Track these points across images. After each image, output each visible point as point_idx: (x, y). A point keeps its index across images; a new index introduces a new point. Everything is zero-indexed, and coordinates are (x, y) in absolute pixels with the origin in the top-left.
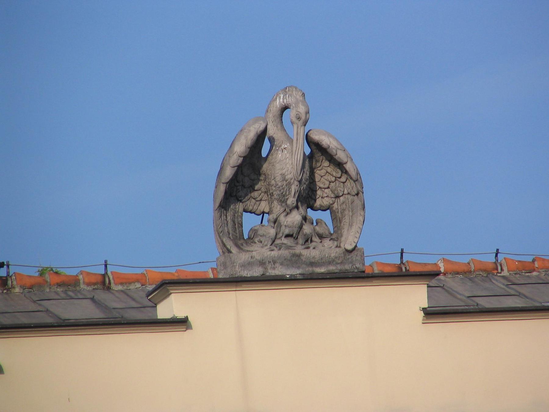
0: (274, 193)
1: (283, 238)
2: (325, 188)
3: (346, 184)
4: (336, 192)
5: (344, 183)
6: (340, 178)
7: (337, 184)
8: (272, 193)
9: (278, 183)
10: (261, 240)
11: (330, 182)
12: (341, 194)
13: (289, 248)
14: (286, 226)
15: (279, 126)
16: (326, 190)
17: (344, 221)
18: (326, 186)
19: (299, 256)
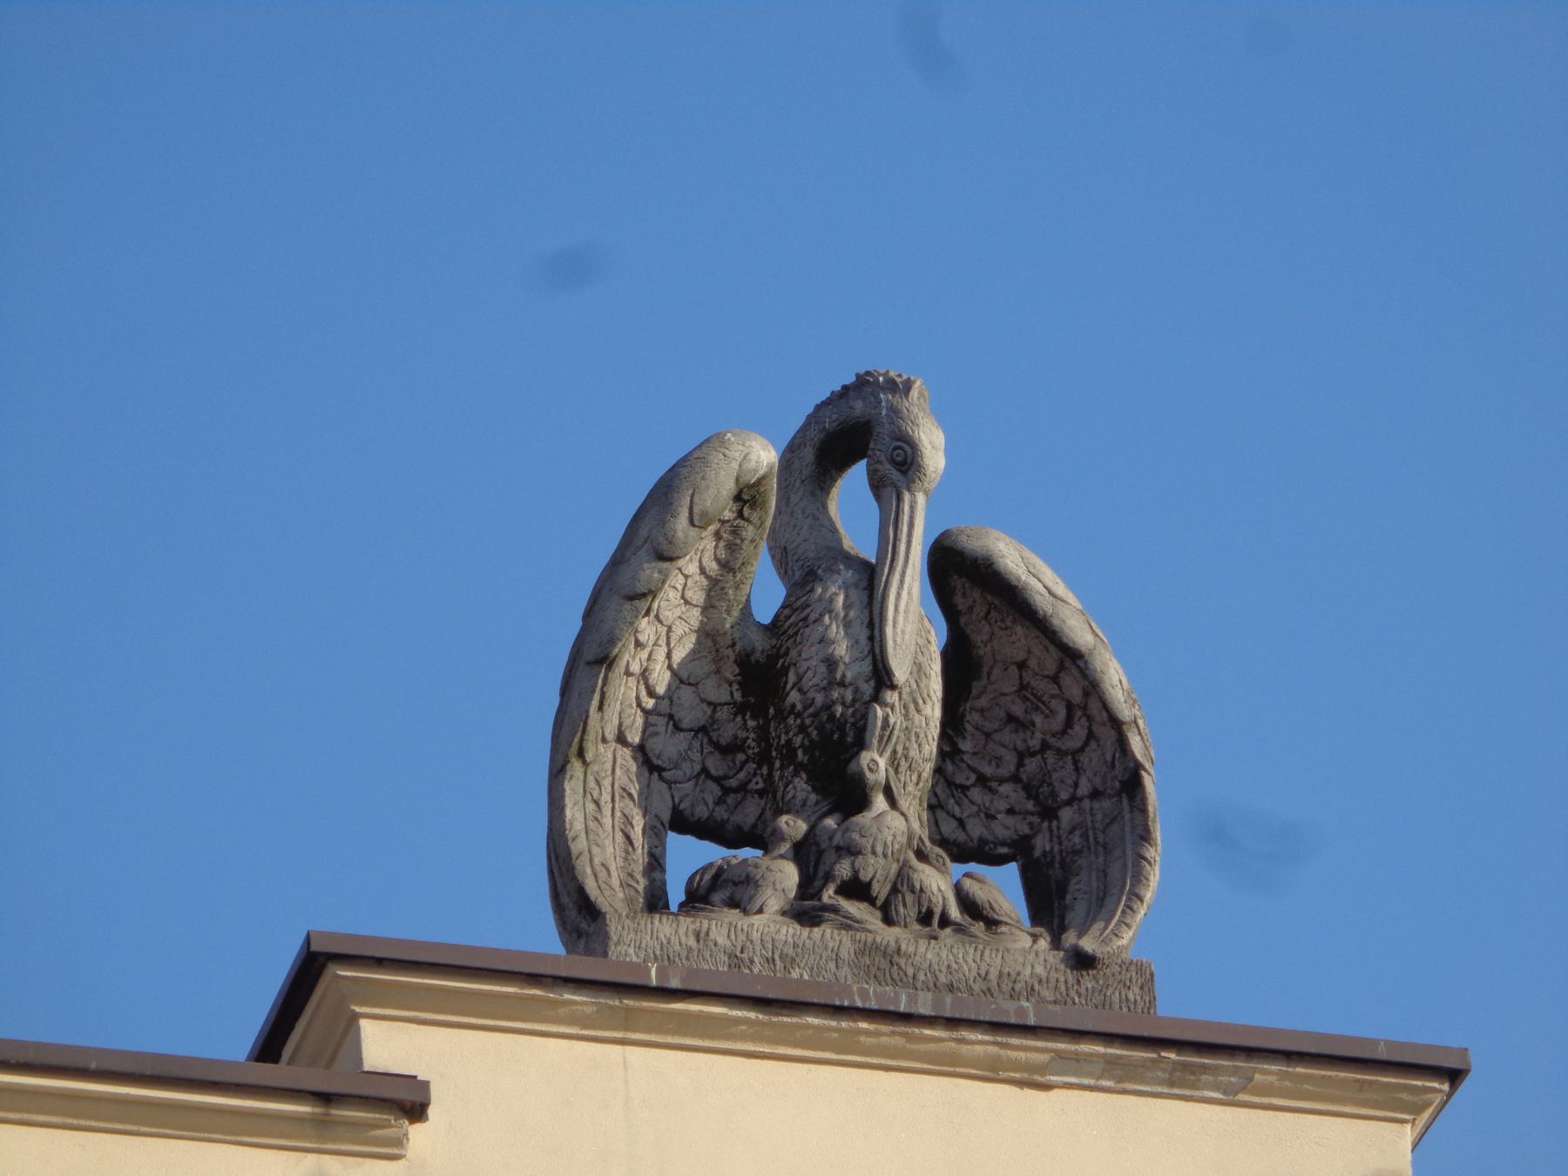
2: (1002, 781)
6: (1064, 732)
14: (838, 848)
16: (1006, 789)
18: (1005, 772)
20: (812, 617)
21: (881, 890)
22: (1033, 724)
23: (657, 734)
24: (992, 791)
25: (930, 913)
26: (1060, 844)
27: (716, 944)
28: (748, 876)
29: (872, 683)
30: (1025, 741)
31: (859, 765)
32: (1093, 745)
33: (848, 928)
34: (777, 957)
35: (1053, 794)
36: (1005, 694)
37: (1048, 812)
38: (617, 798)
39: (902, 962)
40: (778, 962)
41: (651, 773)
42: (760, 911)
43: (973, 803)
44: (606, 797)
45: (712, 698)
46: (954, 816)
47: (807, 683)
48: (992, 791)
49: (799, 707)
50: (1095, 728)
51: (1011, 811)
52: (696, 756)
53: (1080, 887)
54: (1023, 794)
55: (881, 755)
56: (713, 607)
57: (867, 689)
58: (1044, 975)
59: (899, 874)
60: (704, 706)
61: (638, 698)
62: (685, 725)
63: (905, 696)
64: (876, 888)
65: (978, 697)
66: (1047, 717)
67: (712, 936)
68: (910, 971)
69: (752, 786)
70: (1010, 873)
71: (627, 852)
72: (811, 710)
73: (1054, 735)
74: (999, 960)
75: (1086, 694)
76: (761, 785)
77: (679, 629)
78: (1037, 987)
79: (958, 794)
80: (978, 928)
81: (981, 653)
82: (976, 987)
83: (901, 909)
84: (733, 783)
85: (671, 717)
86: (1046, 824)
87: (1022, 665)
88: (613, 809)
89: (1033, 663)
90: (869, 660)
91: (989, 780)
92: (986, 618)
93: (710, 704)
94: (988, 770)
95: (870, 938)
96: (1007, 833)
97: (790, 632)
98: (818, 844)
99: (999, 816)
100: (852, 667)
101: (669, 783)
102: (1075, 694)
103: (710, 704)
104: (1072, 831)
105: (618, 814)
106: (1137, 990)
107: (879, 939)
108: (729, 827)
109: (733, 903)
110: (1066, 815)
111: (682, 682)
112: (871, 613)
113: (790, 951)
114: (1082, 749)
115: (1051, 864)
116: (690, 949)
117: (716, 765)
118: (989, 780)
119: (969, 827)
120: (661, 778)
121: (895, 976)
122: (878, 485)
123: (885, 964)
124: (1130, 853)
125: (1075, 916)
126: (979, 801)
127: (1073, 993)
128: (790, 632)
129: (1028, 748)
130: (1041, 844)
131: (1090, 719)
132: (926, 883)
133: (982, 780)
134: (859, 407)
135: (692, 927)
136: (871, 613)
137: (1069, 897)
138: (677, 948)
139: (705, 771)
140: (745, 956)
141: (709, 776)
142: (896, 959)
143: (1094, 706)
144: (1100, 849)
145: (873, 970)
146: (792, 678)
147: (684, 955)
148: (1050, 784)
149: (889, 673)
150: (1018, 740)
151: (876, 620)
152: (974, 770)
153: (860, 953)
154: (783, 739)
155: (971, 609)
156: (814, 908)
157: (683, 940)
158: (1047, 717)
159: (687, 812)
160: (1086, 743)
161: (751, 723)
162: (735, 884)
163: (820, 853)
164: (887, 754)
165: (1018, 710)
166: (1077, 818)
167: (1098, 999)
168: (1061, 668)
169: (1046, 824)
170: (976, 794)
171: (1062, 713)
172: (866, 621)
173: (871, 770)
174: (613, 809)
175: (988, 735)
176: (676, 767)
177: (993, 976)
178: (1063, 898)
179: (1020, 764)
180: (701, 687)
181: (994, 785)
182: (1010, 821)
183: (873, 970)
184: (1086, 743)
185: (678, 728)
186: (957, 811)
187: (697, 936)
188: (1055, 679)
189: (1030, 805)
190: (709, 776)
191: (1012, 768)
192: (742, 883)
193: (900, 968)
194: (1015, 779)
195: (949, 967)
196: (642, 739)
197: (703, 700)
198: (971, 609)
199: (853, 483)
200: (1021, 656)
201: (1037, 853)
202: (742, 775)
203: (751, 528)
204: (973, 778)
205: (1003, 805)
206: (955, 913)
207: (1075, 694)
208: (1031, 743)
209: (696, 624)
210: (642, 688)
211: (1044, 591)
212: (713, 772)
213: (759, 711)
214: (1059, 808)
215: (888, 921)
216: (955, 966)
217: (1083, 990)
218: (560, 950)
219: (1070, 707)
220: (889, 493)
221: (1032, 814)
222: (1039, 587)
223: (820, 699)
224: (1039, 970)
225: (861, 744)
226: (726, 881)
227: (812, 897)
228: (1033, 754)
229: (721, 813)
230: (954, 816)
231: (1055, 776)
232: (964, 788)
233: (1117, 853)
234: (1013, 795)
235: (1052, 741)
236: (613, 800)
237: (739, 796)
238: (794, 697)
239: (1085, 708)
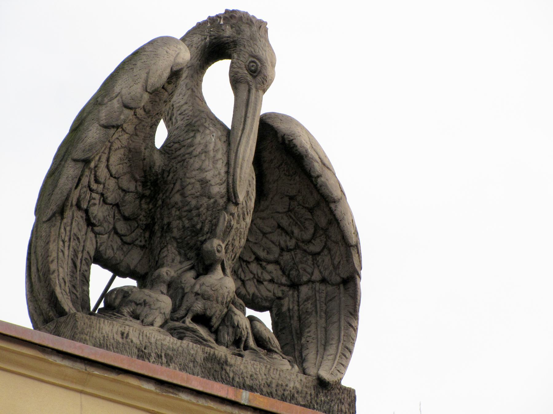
0: (175, 224)
1: (188, 320)
2: (269, 262)
3: (319, 258)
4: (294, 273)
5: (315, 255)
6: (309, 242)
7: (299, 256)
8: (169, 224)
9: (189, 199)
10: (138, 312)
11: (282, 250)
12: (305, 279)
13: (200, 341)
14: (197, 294)
15: (81, 128)
16: (270, 267)
17: (306, 335)
18: (271, 257)
19: (223, 363)
20: (195, 153)
21: (215, 322)
22: (293, 233)
23: (95, 204)
24: (264, 268)
25: (240, 338)
26: (298, 306)
27: (132, 341)
28: (145, 301)
29: (225, 199)
30: (285, 241)
31: (212, 244)
32: (326, 252)
33: (201, 343)
34: (163, 355)
35: (298, 275)
36: (279, 212)
37: (295, 286)
38: (72, 240)
39: (228, 368)
40: (163, 358)
41: (88, 226)
42: (152, 324)
43: (251, 272)
44: (67, 239)
45: (125, 188)
46: (240, 279)
47: (189, 190)
48: (264, 268)
49: (180, 204)
50: (329, 243)
51: (272, 281)
52: (111, 220)
53: (312, 334)
54: (280, 273)
55: (223, 243)
56: (136, 135)
57: (222, 202)
58: (300, 389)
59: (227, 314)
60: (120, 191)
61: (89, 182)
62: (110, 200)
63: (239, 209)
64: (214, 320)
65: (263, 211)
66: (301, 231)
67: (130, 337)
68: (231, 375)
69: (137, 242)
70: (267, 314)
71: (73, 272)
72: (186, 208)
73: (303, 242)
74: (277, 376)
75: (330, 223)
76: (143, 243)
77: (116, 145)
78: (296, 395)
79: (244, 265)
80: (262, 352)
81: (271, 186)
82: (264, 390)
83: (226, 336)
84: (128, 239)
85: (102, 195)
86: (291, 292)
87: (292, 198)
88: (69, 245)
89: (300, 198)
90: (224, 185)
91: (261, 260)
92: (278, 167)
93: (123, 190)
94: (262, 254)
95: (212, 350)
96: (270, 295)
97: (179, 159)
98: (183, 289)
99: (265, 283)
100: (218, 189)
101: (96, 234)
102: (323, 222)
103: (123, 190)
104: (307, 299)
105: (71, 249)
106: (347, 406)
107: (216, 352)
108: (124, 264)
109: (136, 317)
110: (305, 290)
111: (111, 175)
112: (228, 157)
113: (170, 353)
114: (319, 254)
115: (291, 317)
116: (118, 343)
117: (122, 227)
118: (261, 260)
119: (248, 286)
120: (93, 230)
121: (223, 377)
122: (235, 81)
123: (218, 368)
124: (343, 323)
125: (311, 355)
126: (255, 272)
127: (313, 402)
128: (179, 159)
129: (287, 246)
130: (287, 304)
131: (328, 237)
132: (241, 323)
133: (258, 259)
134: (228, 32)
135: (120, 329)
136: (228, 157)
137: (303, 340)
138: (112, 341)
139: (114, 229)
140: (146, 351)
141: (116, 233)
142: (225, 366)
143: (333, 231)
144: (323, 314)
145: (212, 371)
146: (178, 187)
147: (115, 345)
148: (297, 270)
149: (236, 196)
150: (283, 240)
151: (232, 163)
152: (254, 253)
153: (206, 359)
154: (166, 221)
155: (271, 161)
156: (181, 328)
157: (115, 336)
158: (301, 231)
159: (103, 252)
160: (322, 251)
161: (144, 206)
162: (137, 304)
163: (184, 295)
164: (226, 243)
165: (285, 222)
166: (310, 293)
167: (326, 407)
168: (318, 204)
169: (291, 292)
170: (254, 267)
171: (312, 231)
172: (225, 162)
173: (219, 251)
174: (69, 245)
175: (264, 234)
176: (101, 225)
177: (274, 385)
178: (300, 339)
179: (281, 255)
180: (120, 180)
181: (264, 264)
182: (271, 286)
183: (212, 371)
184: (322, 251)
185: (105, 202)
186: (243, 277)
187: (122, 334)
188: (311, 210)
189: (284, 280)
190: (116, 233)
191: (277, 256)
192: (140, 304)
193: (226, 373)
194: (277, 262)
195: (251, 376)
196: (87, 207)
197: (120, 188)
198: (271, 161)
199: (218, 73)
200: (293, 193)
201: (285, 309)
202: (133, 235)
203: (166, 94)
204: (253, 257)
205: (268, 277)
206: (252, 343)
207: (323, 222)
208: (289, 244)
209: (125, 143)
210: (92, 176)
211: (319, 160)
212: (119, 231)
213: (152, 198)
214: (301, 285)
215: (217, 341)
216: (255, 376)
217: (319, 401)
218: (28, 324)
219: (316, 227)
220: (243, 88)
221: (285, 285)
222: (317, 157)
223: (193, 203)
224: (298, 386)
225: (212, 233)
226: (131, 301)
227: (178, 320)
228: (289, 250)
229: (119, 255)
230: (240, 279)
231: (300, 266)
232: (248, 263)
233: (335, 318)
234: (274, 272)
235: (301, 244)
236: (70, 239)
237: (130, 247)
238: (177, 198)
239: (325, 230)
